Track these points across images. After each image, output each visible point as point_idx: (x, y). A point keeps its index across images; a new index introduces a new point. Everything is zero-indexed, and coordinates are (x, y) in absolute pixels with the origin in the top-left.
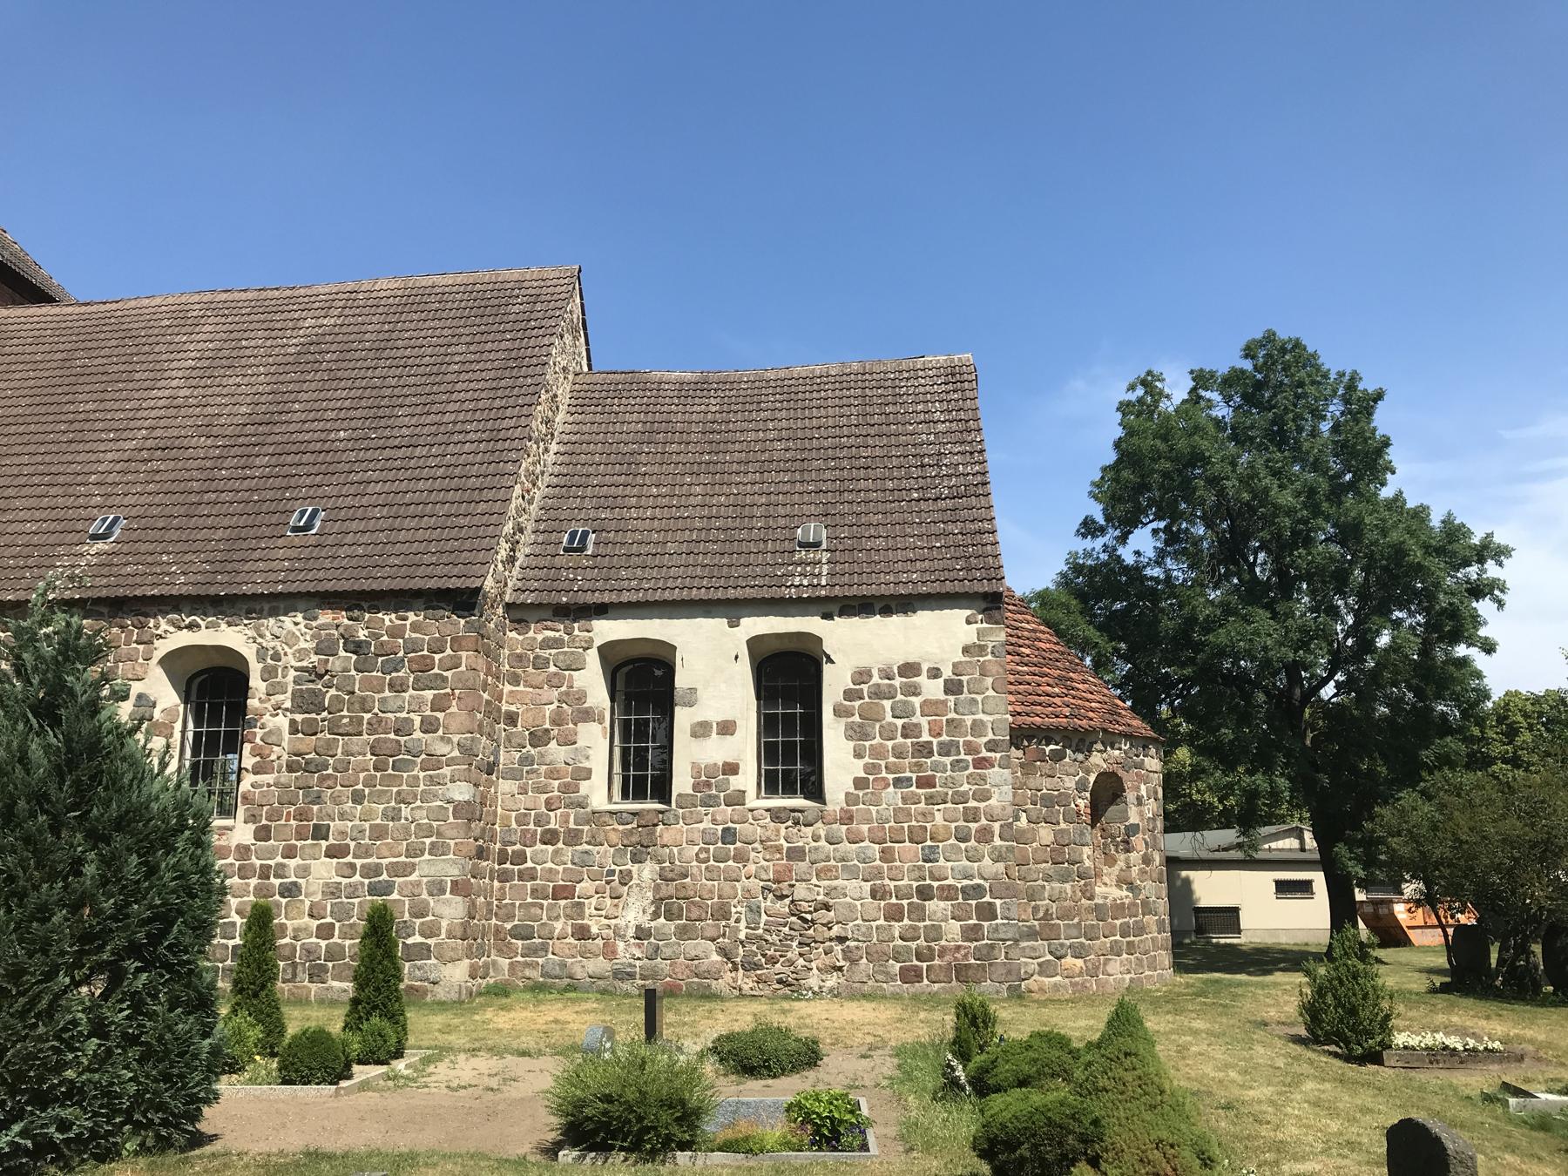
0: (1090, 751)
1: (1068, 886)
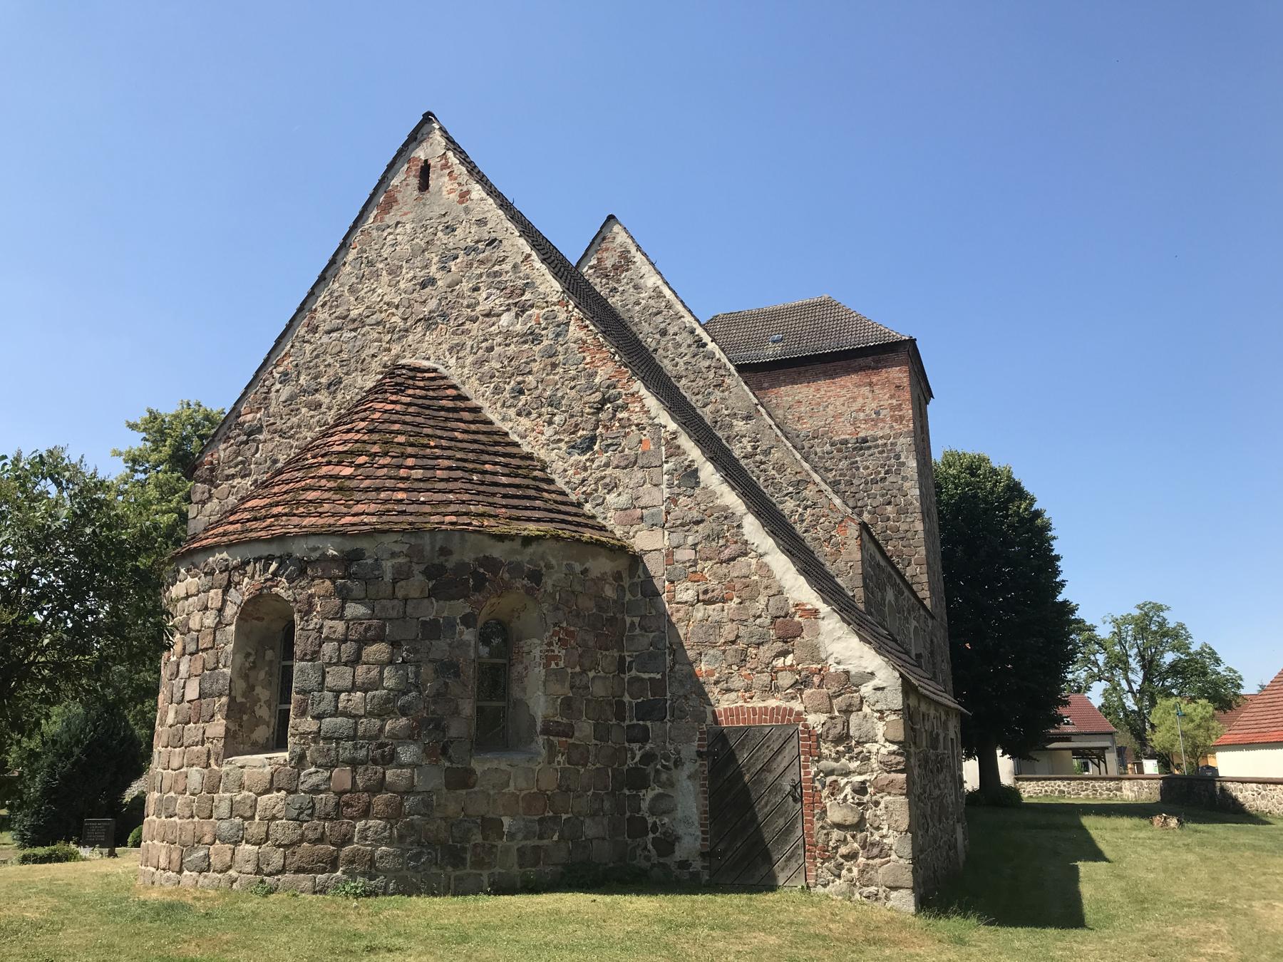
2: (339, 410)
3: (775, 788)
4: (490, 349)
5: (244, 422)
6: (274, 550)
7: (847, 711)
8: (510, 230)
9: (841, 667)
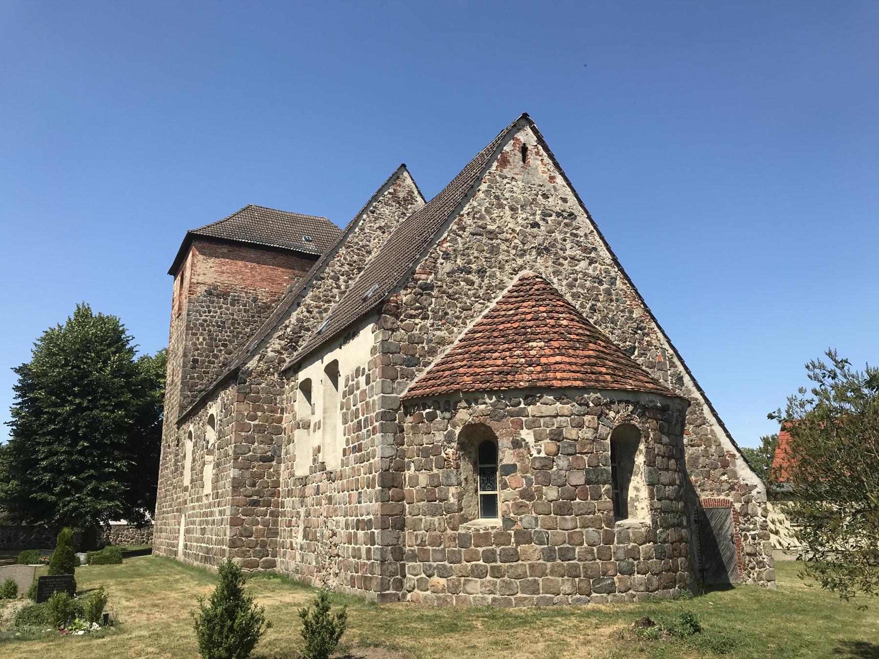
0: (455, 409)
1: (436, 519)
2: (487, 290)
3: (725, 538)
4: (576, 280)
5: (419, 279)
6: (630, 397)
7: (747, 503)
8: (581, 213)
9: (745, 482)
